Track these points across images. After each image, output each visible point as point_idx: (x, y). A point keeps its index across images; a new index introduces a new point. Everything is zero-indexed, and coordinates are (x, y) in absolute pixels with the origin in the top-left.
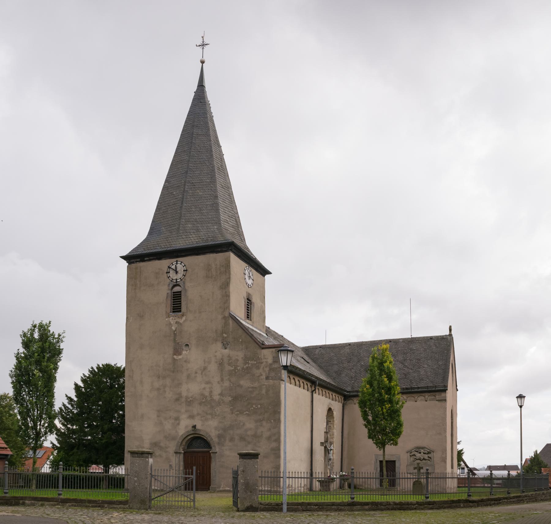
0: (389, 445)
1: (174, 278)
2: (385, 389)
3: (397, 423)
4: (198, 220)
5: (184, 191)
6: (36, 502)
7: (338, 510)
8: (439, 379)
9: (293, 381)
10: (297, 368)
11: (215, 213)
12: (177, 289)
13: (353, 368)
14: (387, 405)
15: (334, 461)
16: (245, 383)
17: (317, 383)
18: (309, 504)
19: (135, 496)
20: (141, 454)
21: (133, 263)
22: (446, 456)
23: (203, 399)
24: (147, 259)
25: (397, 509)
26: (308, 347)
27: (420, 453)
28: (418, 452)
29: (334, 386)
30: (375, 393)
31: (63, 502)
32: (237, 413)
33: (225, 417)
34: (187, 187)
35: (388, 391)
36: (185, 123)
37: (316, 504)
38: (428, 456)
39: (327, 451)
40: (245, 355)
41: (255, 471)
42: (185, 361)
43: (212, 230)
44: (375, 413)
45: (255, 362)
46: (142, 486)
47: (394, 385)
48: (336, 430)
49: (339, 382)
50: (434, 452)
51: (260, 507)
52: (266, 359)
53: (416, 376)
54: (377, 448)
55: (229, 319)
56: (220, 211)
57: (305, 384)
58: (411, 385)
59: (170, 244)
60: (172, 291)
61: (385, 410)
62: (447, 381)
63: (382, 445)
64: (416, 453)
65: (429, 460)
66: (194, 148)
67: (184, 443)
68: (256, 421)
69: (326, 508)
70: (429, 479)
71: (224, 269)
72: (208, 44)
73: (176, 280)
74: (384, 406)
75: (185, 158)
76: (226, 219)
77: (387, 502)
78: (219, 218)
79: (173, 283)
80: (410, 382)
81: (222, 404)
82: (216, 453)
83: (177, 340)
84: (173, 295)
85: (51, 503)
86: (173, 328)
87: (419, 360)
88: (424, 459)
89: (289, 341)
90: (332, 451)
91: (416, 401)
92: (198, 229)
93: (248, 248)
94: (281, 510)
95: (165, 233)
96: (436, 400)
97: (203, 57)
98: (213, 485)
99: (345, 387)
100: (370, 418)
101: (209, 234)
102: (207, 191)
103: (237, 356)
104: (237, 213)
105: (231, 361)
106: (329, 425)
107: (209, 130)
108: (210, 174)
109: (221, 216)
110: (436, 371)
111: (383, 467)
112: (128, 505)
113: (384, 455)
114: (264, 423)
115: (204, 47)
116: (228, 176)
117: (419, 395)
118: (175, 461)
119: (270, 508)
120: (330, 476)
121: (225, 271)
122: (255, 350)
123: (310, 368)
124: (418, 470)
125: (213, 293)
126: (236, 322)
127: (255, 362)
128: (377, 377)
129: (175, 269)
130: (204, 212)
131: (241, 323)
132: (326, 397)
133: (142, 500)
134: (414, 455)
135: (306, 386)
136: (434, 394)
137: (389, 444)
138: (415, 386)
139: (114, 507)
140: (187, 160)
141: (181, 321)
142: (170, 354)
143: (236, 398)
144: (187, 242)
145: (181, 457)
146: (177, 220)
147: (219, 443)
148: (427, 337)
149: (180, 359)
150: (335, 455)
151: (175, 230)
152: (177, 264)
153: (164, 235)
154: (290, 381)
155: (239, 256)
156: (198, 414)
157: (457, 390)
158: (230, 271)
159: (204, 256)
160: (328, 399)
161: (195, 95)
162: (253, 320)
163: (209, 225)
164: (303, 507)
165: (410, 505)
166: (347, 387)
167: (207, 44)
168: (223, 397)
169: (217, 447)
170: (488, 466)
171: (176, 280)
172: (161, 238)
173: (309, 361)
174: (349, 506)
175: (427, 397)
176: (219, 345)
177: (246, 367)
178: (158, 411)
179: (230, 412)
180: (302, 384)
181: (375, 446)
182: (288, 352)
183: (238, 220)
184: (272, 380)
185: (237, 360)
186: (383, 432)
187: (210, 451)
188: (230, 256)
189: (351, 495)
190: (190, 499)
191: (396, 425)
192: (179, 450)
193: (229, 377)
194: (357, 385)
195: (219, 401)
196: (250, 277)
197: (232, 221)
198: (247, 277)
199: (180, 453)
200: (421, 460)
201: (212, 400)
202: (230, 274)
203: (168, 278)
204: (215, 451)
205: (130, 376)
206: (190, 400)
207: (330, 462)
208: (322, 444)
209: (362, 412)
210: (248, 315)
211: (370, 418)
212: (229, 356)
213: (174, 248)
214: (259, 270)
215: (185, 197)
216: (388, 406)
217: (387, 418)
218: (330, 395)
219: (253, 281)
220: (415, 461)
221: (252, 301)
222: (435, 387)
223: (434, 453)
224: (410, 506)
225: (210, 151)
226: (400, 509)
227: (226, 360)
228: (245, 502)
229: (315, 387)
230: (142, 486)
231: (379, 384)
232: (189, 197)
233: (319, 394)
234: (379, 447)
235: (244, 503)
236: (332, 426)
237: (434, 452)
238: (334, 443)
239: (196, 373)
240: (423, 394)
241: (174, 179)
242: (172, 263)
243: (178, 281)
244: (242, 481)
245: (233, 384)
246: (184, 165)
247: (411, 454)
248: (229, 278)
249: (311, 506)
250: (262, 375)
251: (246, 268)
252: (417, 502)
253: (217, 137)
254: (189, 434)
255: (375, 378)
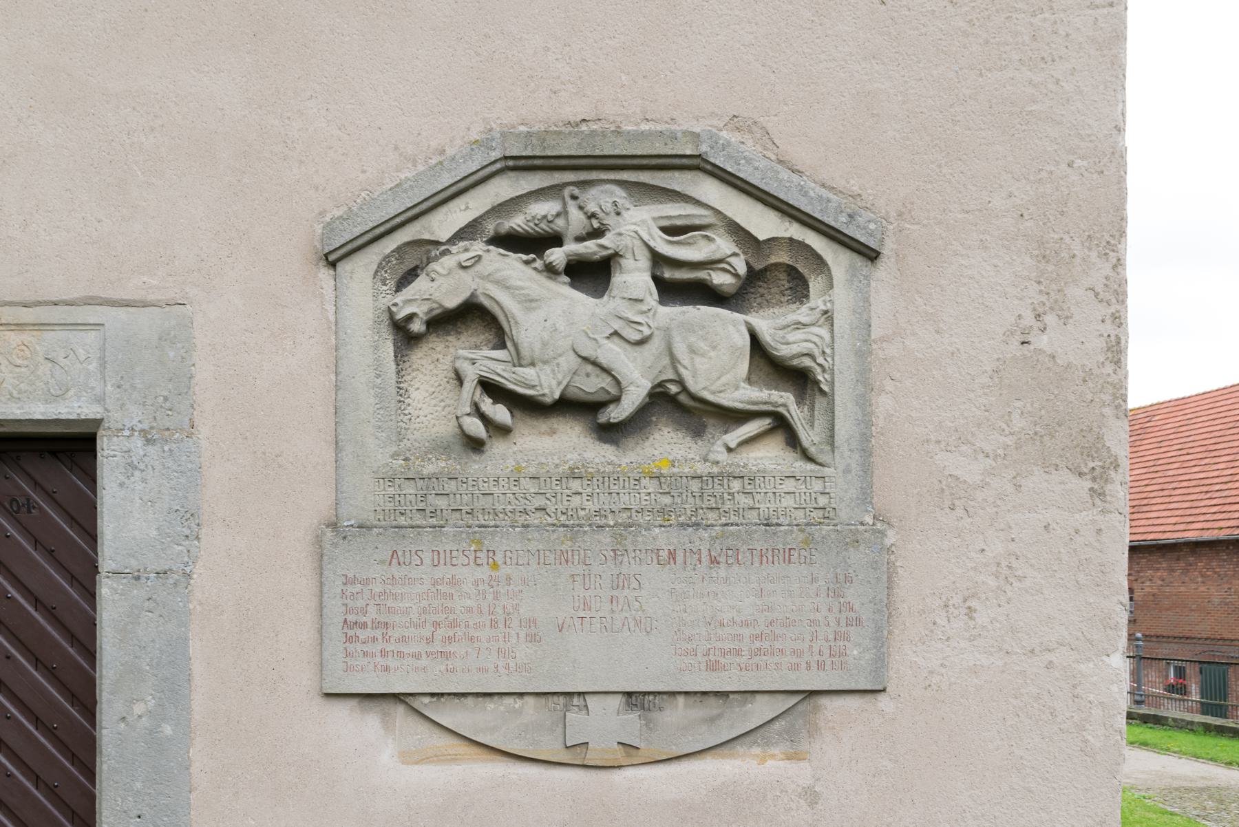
28: (557, 256)
38: (756, 344)
64: (512, 265)
65: (781, 425)
200: (610, 433)
220: (497, 448)
223: (884, 271)
237: (870, 255)
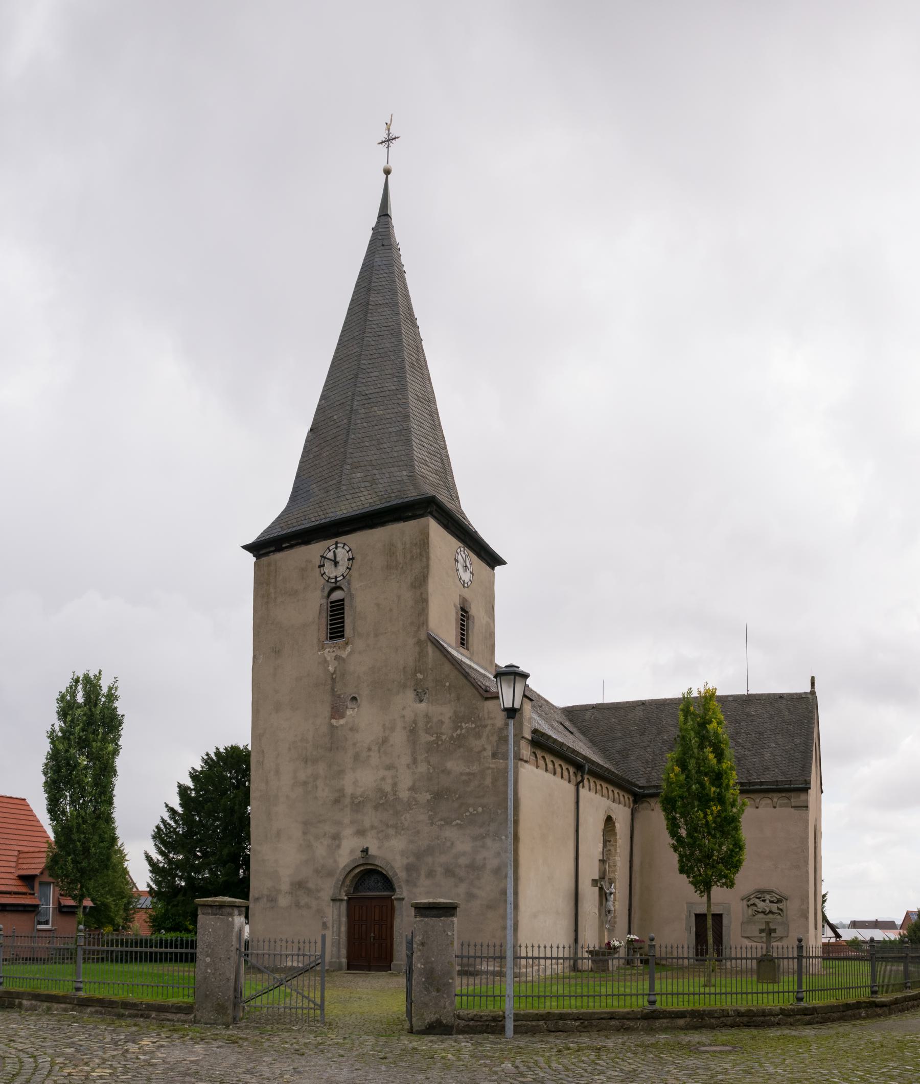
0: (718, 886)
1: (332, 576)
2: (710, 776)
3: (733, 843)
4: (374, 463)
5: (351, 411)
6: (39, 1004)
7: (622, 1030)
8: (796, 769)
9: (541, 762)
10: (550, 737)
11: (404, 447)
12: (337, 595)
13: (649, 746)
14: (714, 808)
15: (616, 914)
16: (455, 765)
17: (587, 769)
18: (562, 1017)
19: (207, 996)
20: (218, 907)
21: (267, 554)
22: (808, 908)
23: (381, 798)
24: (287, 545)
25: (742, 1024)
26: (573, 707)
27: (764, 901)
29: (617, 776)
30: (692, 782)
31: (82, 1005)
32: (440, 823)
33: (418, 832)
34: (356, 403)
35: (715, 779)
36: (356, 287)
37: (577, 1017)
39: (604, 896)
40: (455, 712)
41: (448, 945)
42: (351, 729)
43: (399, 478)
44: (693, 822)
45: (474, 726)
46: (220, 974)
47: (727, 767)
48: (619, 856)
49: (624, 771)
50: (787, 900)
51: (456, 1024)
52: (492, 719)
53: (758, 762)
54: (696, 892)
55: (427, 645)
56: (414, 443)
57: (564, 768)
58: (749, 778)
59: (325, 512)
60: (329, 601)
61: (710, 818)
62: (810, 773)
63: (704, 885)
64: (757, 900)
66: (369, 330)
67: (348, 882)
68: (475, 838)
69: (596, 1026)
70: (804, 960)
71: (418, 551)
72: (398, 138)
73: (336, 577)
74: (709, 809)
75: (355, 351)
76: (423, 457)
77: (723, 1010)
78: (411, 456)
79: (329, 584)
80: (746, 772)
81: (414, 807)
82: (403, 899)
83: (337, 691)
84: (331, 607)
85: (63, 1006)
86: (331, 669)
87: (761, 733)
88: (771, 912)
89: (539, 695)
90: (612, 896)
91: (757, 808)
92: (375, 478)
93: (463, 513)
94: (501, 1031)
95: (317, 494)
96: (792, 807)
97: (388, 163)
98: (396, 961)
99: (635, 780)
100: (683, 832)
101: (393, 487)
102: (390, 407)
103: (441, 714)
104: (445, 448)
105: (430, 724)
106: (609, 847)
107: (395, 294)
108: (397, 375)
109: (415, 453)
110: (790, 754)
111: (708, 930)
112: (193, 1015)
113: (709, 906)
114: (489, 842)
115: (391, 144)
116: (430, 380)
117: (762, 795)
118: (333, 915)
119: (477, 1026)
120: (609, 943)
121: (421, 555)
122: (473, 702)
123: (574, 742)
124: (767, 934)
125: (399, 597)
126: (440, 650)
127: (474, 726)
128: (696, 751)
129: (333, 559)
130: (386, 447)
131: (448, 652)
132: (602, 796)
133: (219, 1004)
134: (754, 904)
135: (566, 774)
136: (788, 795)
137: (719, 884)
138: (755, 779)
139: (168, 1018)
140: (357, 354)
141: (344, 654)
142: (325, 718)
143: (438, 796)
144: (354, 505)
145: (342, 907)
146: (338, 467)
147: (407, 881)
148: (774, 694)
149: (342, 725)
150: (618, 903)
151: (334, 487)
152: (336, 548)
153: (316, 498)
154: (537, 761)
155: (446, 527)
156: (372, 827)
157: (822, 792)
158: (428, 552)
159: (382, 528)
160: (606, 799)
161: (373, 234)
162: (471, 649)
163: (392, 469)
164: (549, 1022)
165: (769, 1015)
166: (638, 779)
167: (395, 138)
168: (416, 794)
169: (404, 888)
170: (851, 922)
171: (336, 577)
172: (311, 504)
173: (574, 730)
174: (645, 1019)
175: (775, 800)
176: (410, 694)
177: (457, 735)
178: (306, 823)
179: (428, 822)
180: (558, 770)
181: (692, 888)
182: (517, 677)
183: (445, 462)
184: (502, 759)
185: (442, 722)
186: (707, 861)
187: (393, 895)
188: (428, 525)
189: (649, 995)
190: (315, 1004)
191: (731, 846)
192: (340, 894)
193: (427, 755)
194: (657, 776)
195: (408, 800)
196: (466, 566)
197: (435, 463)
198: (460, 567)
199: (342, 900)
200: (766, 914)
201: (397, 799)
202: (428, 558)
203: (322, 575)
204: (401, 897)
205: (258, 761)
206: (359, 802)
207: (609, 917)
208: (595, 882)
209: (668, 819)
210: (462, 639)
211: (683, 832)
212: (427, 716)
213: (332, 519)
214: (483, 554)
215: (353, 422)
216: (716, 809)
217: (715, 834)
218: (610, 792)
219: (473, 575)
221: (470, 613)
222: (789, 782)
223: (788, 901)
224: (769, 1018)
225: (397, 333)
226: (748, 1025)
227: (421, 724)
228: (425, 1013)
229: (582, 776)
230: (220, 974)
231: (698, 765)
232: (359, 421)
233: (590, 789)
234: (700, 890)
235: (423, 1014)
236: (612, 849)
238: (617, 881)
239: (369, 749)
240: (770, 795)
241: (334, 392)
242: (328, 548)
243: (338, 579)
244: (419, 965)
245: (434, 768)
246: (352, 364)
247: (749, 903)
248: (427, 566)
249: (566, 1022)
250: (485, 749)
251: (459, 551)
252: (781, 1009)
253: (410, 308)
254: (356, 864)
255: (691, 752)
